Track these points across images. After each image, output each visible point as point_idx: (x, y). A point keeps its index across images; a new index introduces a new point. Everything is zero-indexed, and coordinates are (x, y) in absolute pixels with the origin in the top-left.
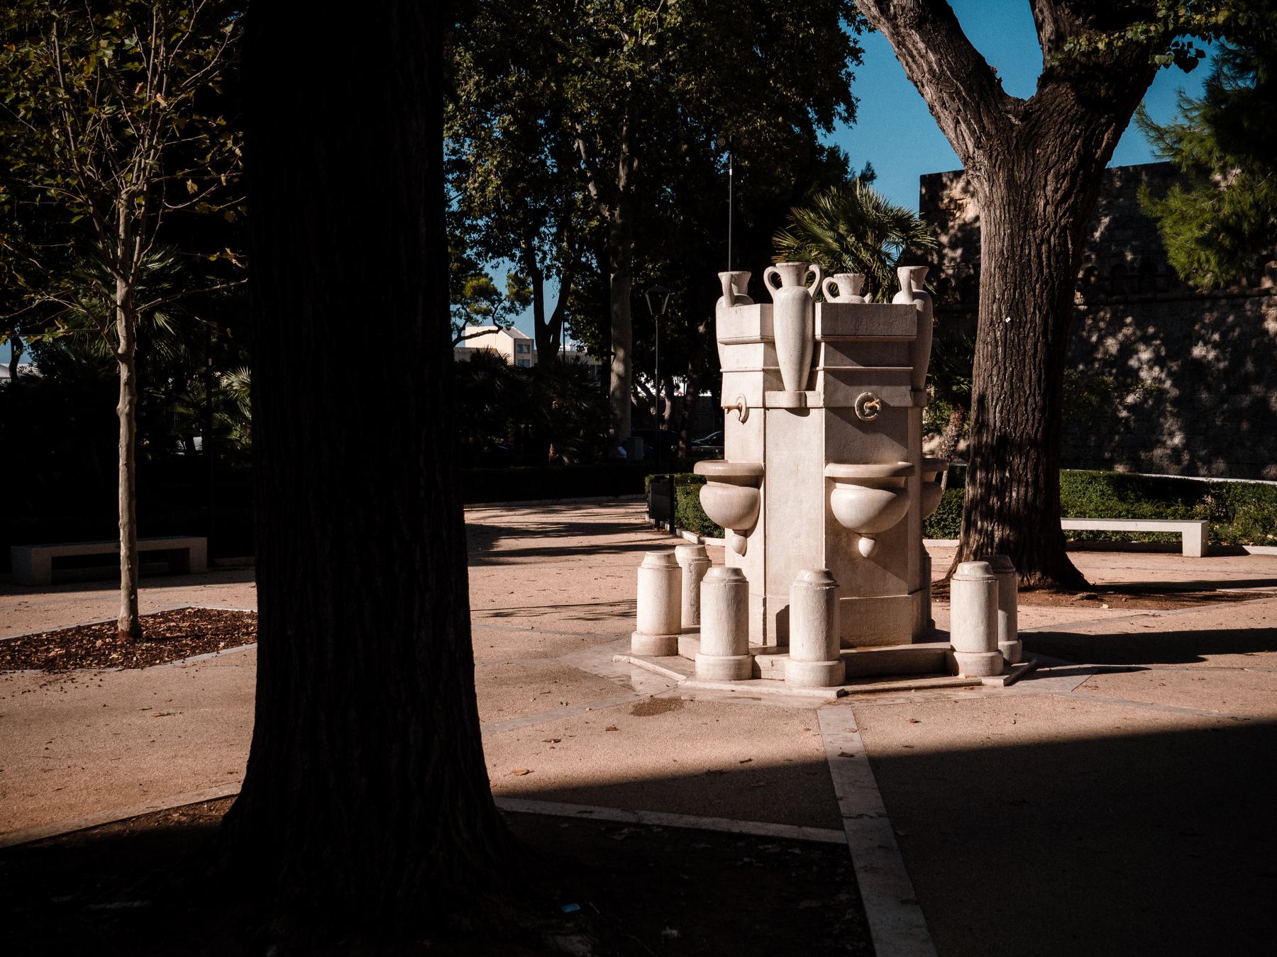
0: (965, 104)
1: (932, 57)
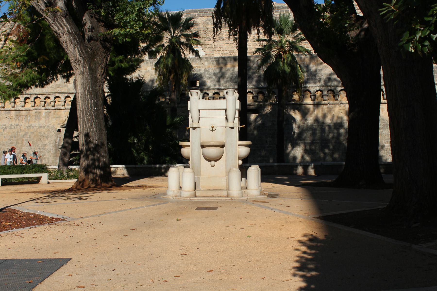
0: (78, 43)
1: (68, 26)
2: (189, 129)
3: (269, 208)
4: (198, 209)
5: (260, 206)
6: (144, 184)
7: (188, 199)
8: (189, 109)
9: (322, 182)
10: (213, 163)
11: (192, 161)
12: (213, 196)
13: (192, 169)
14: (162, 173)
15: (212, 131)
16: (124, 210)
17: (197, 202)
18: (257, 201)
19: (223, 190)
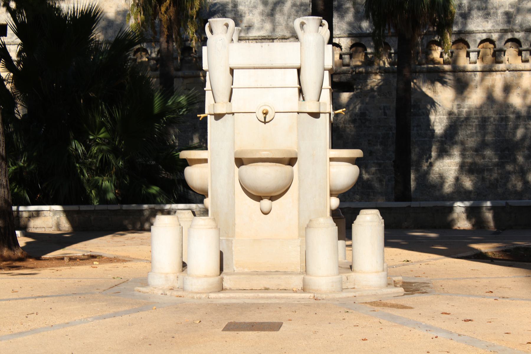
2: (206, 118)
3: (418, 325)
4: (232, 327)
5: (393, 318)
6: (96, 251)
7: (204, 296)
8: (205, 67)
9: (518, 248)
10: (266, 203)
11: (212, 198)
12: (267, 289)
13: (214, 219)
14: (140, 224)
15: (265, 122)
16: (34, 331)
17: (227, 307)
18: (378, 304)
19: (292, 273)
